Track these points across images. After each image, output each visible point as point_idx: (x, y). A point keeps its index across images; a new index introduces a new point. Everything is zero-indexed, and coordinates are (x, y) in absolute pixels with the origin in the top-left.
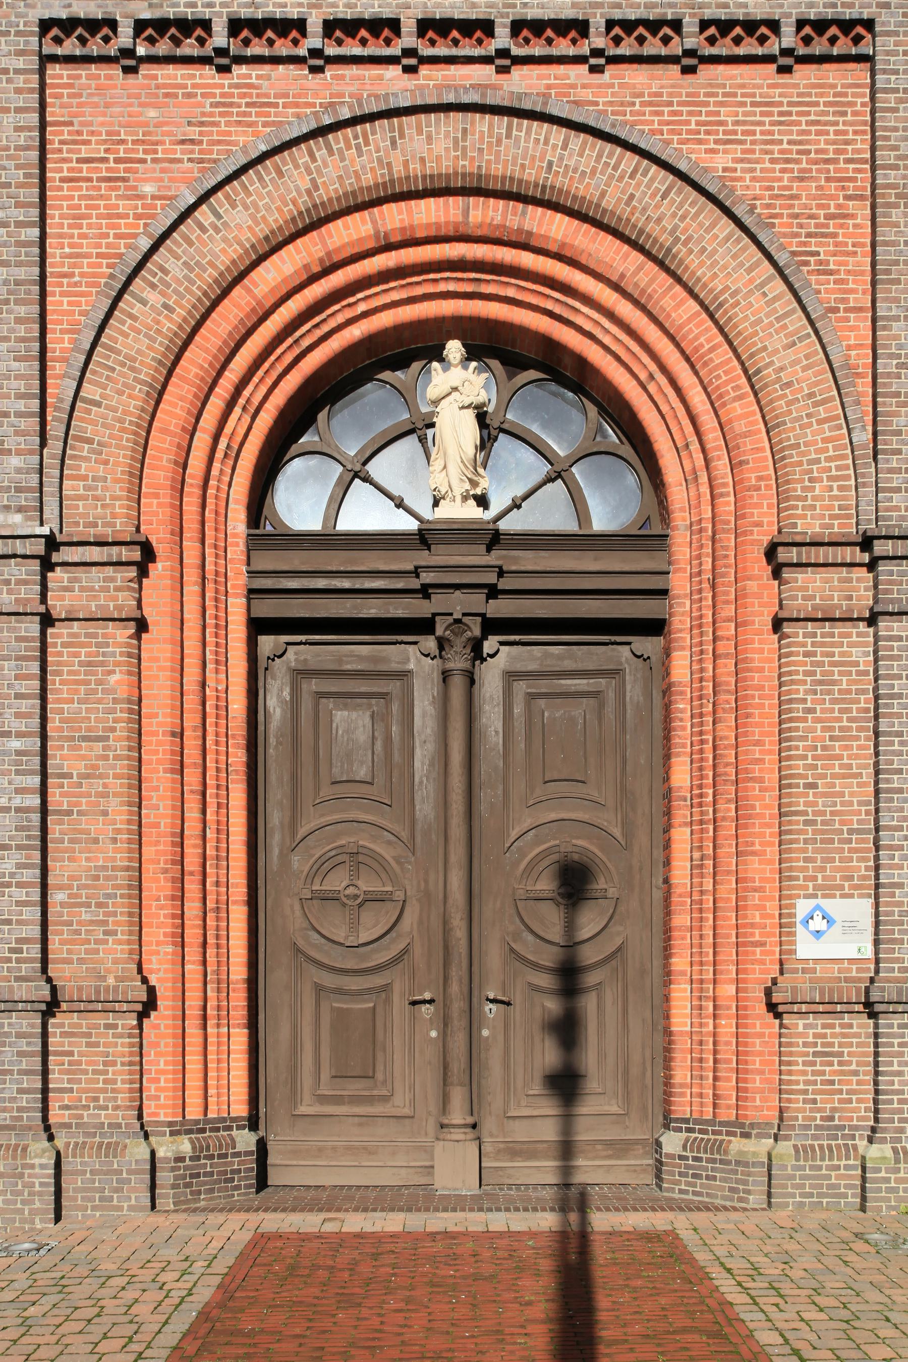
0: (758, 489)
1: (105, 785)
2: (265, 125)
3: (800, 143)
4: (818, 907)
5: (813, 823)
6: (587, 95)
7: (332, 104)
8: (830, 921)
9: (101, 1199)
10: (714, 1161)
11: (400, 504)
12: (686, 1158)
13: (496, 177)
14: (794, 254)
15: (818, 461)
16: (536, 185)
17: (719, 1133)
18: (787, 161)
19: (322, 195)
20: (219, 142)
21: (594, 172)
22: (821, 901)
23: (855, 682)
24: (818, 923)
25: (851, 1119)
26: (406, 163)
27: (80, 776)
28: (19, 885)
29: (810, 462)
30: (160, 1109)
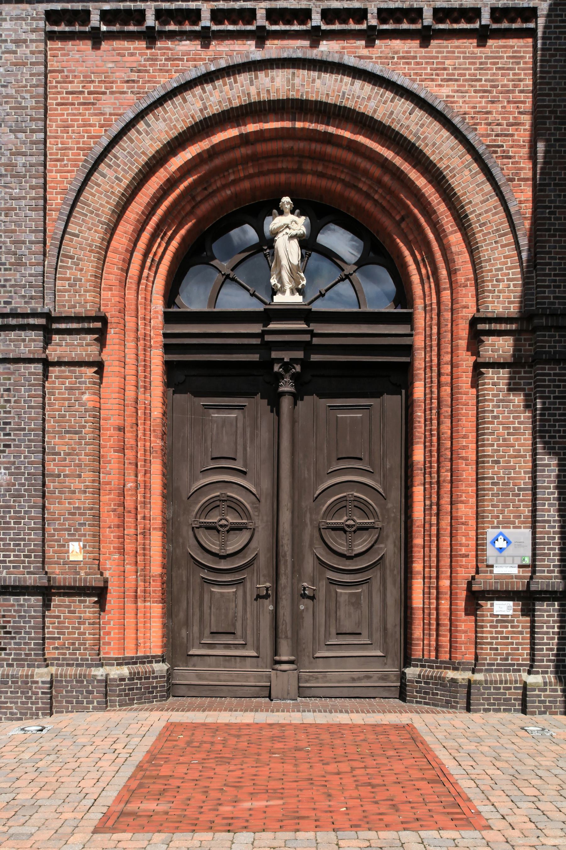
1: (79, 460)
4: (501, 534)
8: (508, 543)
12: (420, 682)
14: (488, 146)
19: (209, 112)
24: (501, 543)
25: (518, 660)
26: (259, 94)
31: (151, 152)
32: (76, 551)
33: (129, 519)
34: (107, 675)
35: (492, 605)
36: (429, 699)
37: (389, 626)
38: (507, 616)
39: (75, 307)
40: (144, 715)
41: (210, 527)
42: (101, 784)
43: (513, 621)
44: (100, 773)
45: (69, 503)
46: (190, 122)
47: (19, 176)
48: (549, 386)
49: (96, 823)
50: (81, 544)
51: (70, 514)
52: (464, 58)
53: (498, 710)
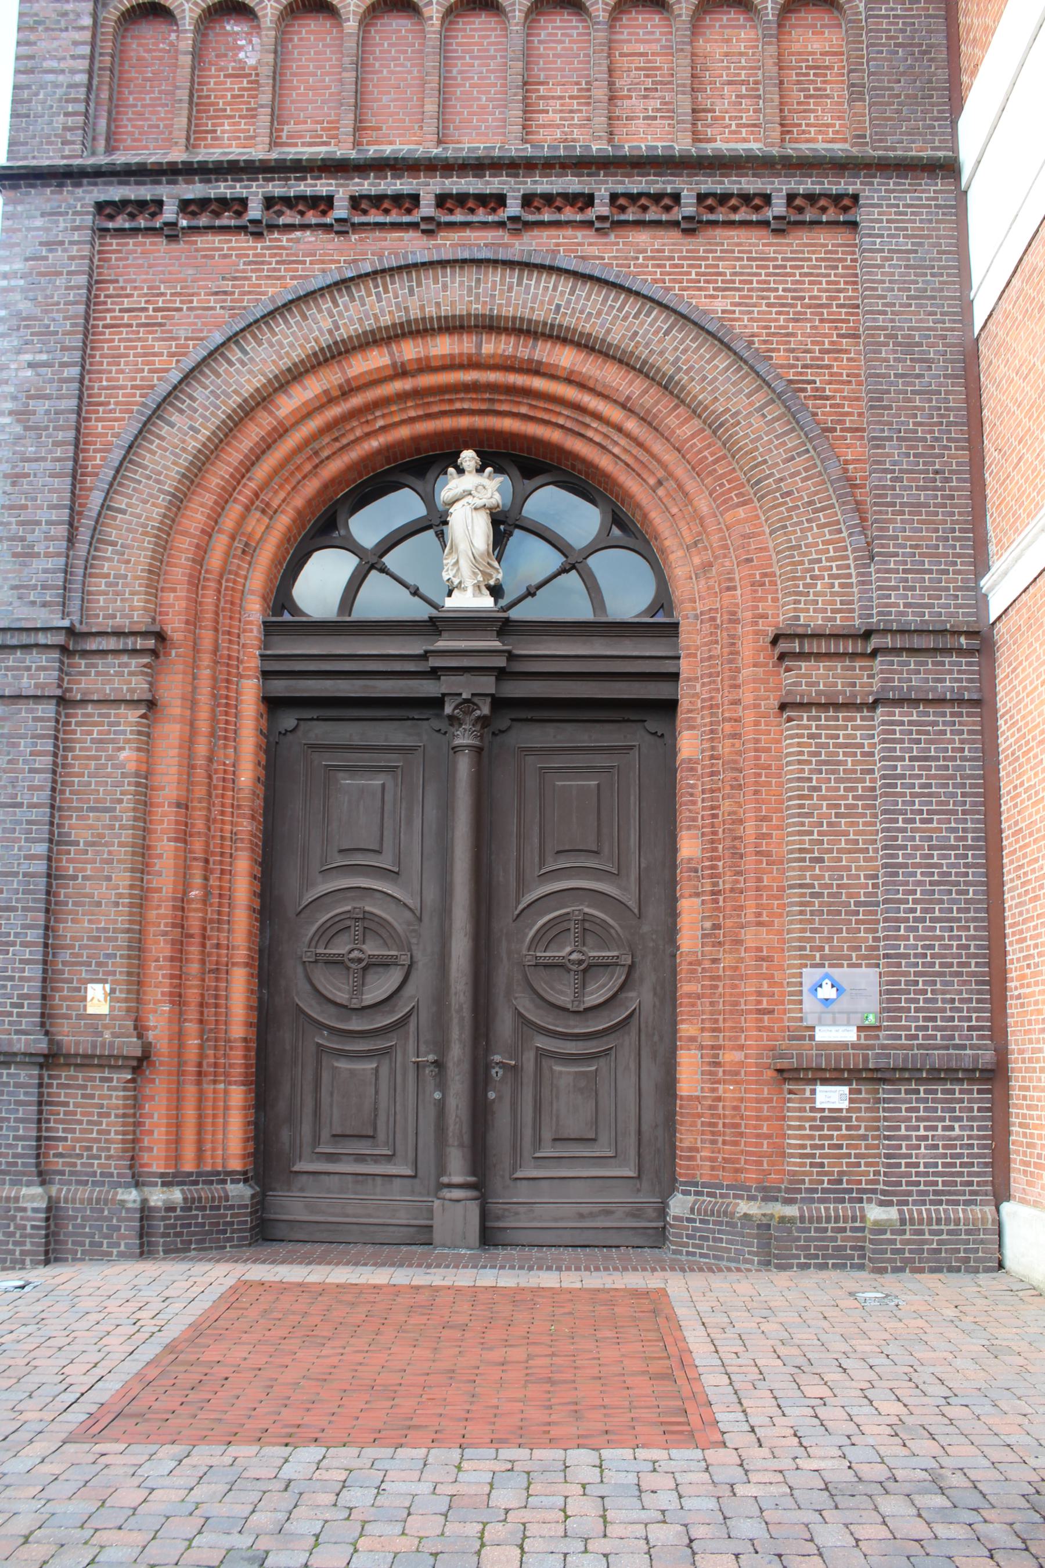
0: (763, 584)
1: (110, 853)
2: (292, 278)
3: (795, 290)
5: (820, 895)
6: (594, 251)
7: (355, 261)
9: (91, 1244)
10: (720, 1223)
11: (416, 593)
12: (694, 1221)
13: (507, 318)
14: (791, 382)
15: (819, 561)
16: (545, 324)
17: (727, 1196)
18: (783, 305)
19: (343, 333)
20: (249, 293)
21: (599, 313)
22: (827, 969)
23: (860, 763)
24: (827, 992)
25: (860, 1182)
26: (422, 308)
27: (87, 844)
28: (24, 944)
29: (811, 562)
30: (155, 1162)
31: (247, 390)
32: (98, 999)
33: (194, 950)
34: (144, 1201)
35: (813, 1092)
36: (709, 1248)
37: (645, 1127)
38: (840, 1110)
39: (114, 617)
40: (200, 1268)
41: (335, 963)
42: (99, 1371)
43: (850, 1119)
44: (101, 1355)
45: (90, 921)
46: (311, 346)
47: (37, 428)
48: (902, 741)
49: (72, 1427)
50: (108, 987)
51: (89, 938)
52: (749, 259)
53: (823, 1267)
